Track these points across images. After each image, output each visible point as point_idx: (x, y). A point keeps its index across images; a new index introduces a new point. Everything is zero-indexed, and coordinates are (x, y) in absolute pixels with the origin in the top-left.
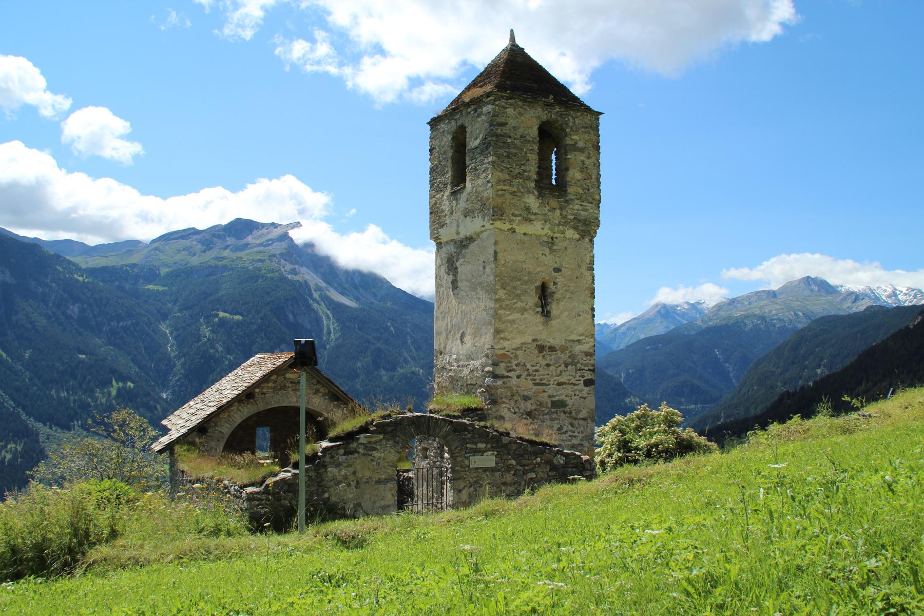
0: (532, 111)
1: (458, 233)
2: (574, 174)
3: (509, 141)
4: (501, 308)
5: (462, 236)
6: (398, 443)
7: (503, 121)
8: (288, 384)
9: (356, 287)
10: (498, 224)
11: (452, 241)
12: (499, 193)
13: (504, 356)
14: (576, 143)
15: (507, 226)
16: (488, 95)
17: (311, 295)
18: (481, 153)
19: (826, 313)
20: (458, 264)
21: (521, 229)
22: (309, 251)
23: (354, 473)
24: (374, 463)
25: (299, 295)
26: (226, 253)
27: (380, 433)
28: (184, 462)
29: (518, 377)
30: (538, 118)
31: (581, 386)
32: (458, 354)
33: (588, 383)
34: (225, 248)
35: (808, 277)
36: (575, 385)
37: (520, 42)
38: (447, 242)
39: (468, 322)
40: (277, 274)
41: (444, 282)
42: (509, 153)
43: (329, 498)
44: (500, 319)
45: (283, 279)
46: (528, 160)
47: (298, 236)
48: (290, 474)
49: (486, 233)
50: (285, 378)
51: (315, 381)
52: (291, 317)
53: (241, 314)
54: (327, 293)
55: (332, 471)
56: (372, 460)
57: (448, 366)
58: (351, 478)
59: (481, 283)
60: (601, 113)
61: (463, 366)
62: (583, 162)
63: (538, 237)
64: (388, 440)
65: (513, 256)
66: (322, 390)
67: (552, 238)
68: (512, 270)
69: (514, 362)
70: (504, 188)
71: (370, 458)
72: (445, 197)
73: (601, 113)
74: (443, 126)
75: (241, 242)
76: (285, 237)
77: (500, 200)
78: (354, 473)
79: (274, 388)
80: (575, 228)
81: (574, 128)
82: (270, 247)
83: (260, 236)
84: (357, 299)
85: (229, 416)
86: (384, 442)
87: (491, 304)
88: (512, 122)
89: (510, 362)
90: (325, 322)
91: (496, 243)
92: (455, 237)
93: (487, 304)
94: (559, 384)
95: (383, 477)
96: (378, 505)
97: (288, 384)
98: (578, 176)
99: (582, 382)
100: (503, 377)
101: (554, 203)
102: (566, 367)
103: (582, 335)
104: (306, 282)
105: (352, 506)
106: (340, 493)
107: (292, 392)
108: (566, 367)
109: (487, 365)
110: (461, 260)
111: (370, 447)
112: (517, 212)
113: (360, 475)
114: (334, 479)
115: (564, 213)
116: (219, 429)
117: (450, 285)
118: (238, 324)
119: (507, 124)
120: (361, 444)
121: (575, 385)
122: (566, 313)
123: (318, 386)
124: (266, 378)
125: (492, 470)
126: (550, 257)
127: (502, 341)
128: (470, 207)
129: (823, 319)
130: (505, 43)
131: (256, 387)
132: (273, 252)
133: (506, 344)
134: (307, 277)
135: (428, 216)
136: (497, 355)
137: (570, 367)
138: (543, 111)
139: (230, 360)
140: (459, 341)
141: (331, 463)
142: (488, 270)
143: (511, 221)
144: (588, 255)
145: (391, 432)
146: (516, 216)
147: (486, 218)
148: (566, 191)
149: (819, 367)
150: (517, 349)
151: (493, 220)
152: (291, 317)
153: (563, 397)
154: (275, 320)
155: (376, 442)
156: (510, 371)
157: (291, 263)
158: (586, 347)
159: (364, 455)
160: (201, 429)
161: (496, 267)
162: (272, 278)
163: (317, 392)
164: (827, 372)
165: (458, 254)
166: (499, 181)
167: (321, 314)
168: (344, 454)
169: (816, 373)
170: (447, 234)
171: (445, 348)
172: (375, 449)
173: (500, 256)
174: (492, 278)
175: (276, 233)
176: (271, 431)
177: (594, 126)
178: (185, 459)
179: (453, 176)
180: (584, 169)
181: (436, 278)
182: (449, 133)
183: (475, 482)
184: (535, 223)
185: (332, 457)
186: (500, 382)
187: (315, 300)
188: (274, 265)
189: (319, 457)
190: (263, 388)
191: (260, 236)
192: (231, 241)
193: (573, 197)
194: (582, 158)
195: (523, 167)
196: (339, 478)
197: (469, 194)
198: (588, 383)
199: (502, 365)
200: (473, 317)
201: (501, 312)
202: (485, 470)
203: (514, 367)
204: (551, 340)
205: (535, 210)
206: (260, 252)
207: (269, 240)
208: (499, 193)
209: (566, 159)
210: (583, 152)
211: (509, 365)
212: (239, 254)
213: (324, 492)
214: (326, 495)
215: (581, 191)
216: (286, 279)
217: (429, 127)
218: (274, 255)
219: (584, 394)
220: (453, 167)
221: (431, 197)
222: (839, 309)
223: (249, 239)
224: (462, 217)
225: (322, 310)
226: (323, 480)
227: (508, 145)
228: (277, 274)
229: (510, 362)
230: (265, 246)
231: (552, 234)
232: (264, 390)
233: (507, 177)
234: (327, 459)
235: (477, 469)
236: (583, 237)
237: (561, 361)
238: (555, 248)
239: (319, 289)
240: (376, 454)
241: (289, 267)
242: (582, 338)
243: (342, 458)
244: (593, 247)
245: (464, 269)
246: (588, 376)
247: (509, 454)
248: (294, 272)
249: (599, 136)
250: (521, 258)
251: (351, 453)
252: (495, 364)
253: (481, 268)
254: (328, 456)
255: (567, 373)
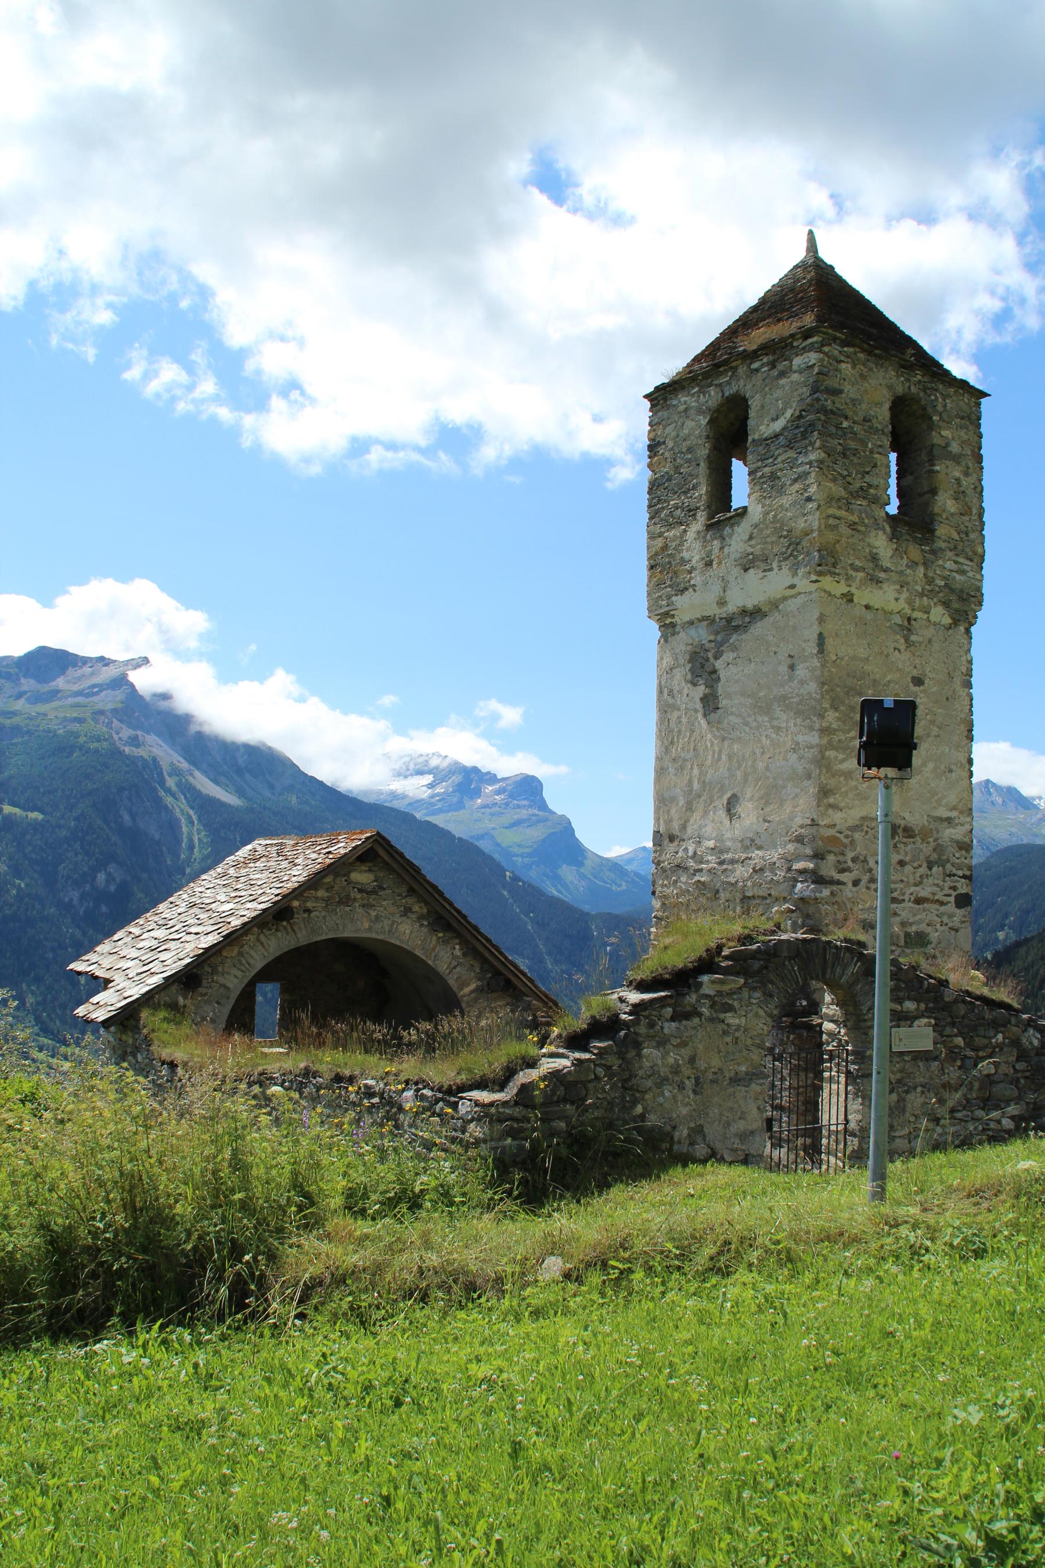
0: (881, 373)
1: (722, 603)
2: (945, 503)
3: (845, 424)
4: (830, 746)
5: (731, 608)
6: (771, 996)
7: (836, 386)
8: (355, 894)
9: (239, 771)
10: (827, 582)
11: (704, 619)
12: (831, 521)
13: (833, 840)
14: (948, 445)
15: (842, 588)
16: (807, 334)
17: (162, 782)
18: (789, 446)
19: (1014, 841)
20: (719, 664)
21: (865, 596)
22: (163, 705)
23: (692, 1060)
24: (728, 1039)
25: (144, 779)
26: (20, 705)
27: (737, 974)
28: (165, 1044)
29: (856, 883)
30: (890, 387)
31: (951, 908)
32: (720, 839)
33: (963, 901)
34: (19, 696)
35: (988, 781)
36: (942, 904)
37: (827, 255)
38: (691, 623)
39: (746, 775)
40: (105, 744)
41: (681, 701)
42: (846, 449)
43: (642, 1117)
44: (828, 768)
45: (116, 753)
46: (875, 466)
47: (142, 680)
48: (566, 1062)
49: (800, 600)
50: (349, 882)
51: (404, 890)
52: (127, 817)
53: (41, 811)
54: (191, 779)
55: (650, 1052)
56: (725, 1033)
57: (691, 863)
58: (687, 1071)
59: (784, 698)
60: (986, 395)
61: (733, 862)
62: (958, 480)
63: (888, 614)
64: (754, 989)
65: (849, 647)
66: (416, 908)
67: (909, 619)
68: (848, 675)
69: (850, 855)
70: (838, 513)
71: (721, 1027)
72: (691, 534)
73: (986, 395)
74: (683, 400)
75: (45, 688)
76: (121, 682)
77: (831, 536)
78: (692, 1060)
79: (327, 901)
80: (946, 604)
81: (945, 416)
82: (95, 699)
83: (79, 679)
84: (240, 793)
85: (241, 954)
86: (745, 993)
87: (814, 738)
88: (850, 391)
89: (843, 854)
90: (185, 829)
91: (821, 619)
92: (713, 610)
93: (800, 738)
94: (919, 901)
95: (743, 1069)
96: (733, 1129)
97: (355, 894)
98: (952, 506)
99: (952, 899)
100: (832, 882)
101: (914, 552)
102: (930, 868)
103: (954, 808)
104: (154, 759)
105: (685, 1132)
106: (669, 1107)
107: (360, 910)
108: (930, 868)
109: (798, 858)
110: (728, 656)
111: (721, 1005)
112: (857, 563)
113: (702, 1064)
114: (653, 1072)
115: (930, 574)
116: (221, 979)
117: (699, 706)
118: (35, 826)
119: (841, 392)
120: (707, 996)
121: (942, 904)
122: (931, 765)
123: (410, 900)
124: (314, 882)
125: (925, 1056)
126: (906, 655)
127: (830, 811)
128: (757, 550)
129: (1010, 849)
130: (799, 254)
131: (296, 898)
132: (100, 706)
133: (837, 817)
134: (156, 751)
135: (644, 573)
136: (822, 838)
137: (935, 869)
138: (898, 376)
139: (19, 888)
140: (722, 814)
141: (651, 1037)
142: (801, 672)
143: (849, 578)
144: (964, 658)
145: (759, 971)
146: (856, 569)
147: (801, 572)
148: (932, 531)
149: (1001, 928)
150: (854, 828)
151: (820, 574)
152: (127, 817)
153: (923, 927)
154: (99, 822)
155: (731, 994)
156: (842, 871)
157: (131, 726)
158: (956, 833)
159: (711, 1020)
160: (189, 978)
161: (823, 666)
162: (97, 751)
163: (407, 911)
164: (1013, 937)
165: (721, 644)
166: (831, 500)
167: (178, 814)
168: (673, 1019)
169: (997, 938)
170: (686, 606)
171: (684, 827)
172: (730, 1008)
173: (829, 643)
174: (813, 687)
175: (107, 674)
176: (284, 991)
177: (974, 417)
178: (166, 1037)
179: (711, 494)
180: (959, 495)
181: (660, 692)
182: (700, 412)
183: (899, 1081)
184: (885, 586)
185: (652, 1025)
186: (826, 892)
187: (169, 791)
188: (101, 729)
189: (626, 1025)
190: (307, 899)
191: (79, 679)
192: (28, 684)
193: (943, 545)
194: (957, 474)
195: (867, 479)
196: (664, 1071)
197: (756, 526)
198: (963, 901)
199: (831, 858)
200: (761, 765)
201: (831, 754)
202: (918, 1056)
203: (850, 863)
204: (907, 815)
205: (886, 563)
206: (78, 705)
207: (94, 686)
208: (831, 521)
209: (932, 471)
210: (958, 463)
211: (841, 858)
212: (41, 708)
213: (634, 1103)
214: (639, 1109)
215: (956, 536)
216: (121, 753)
217: (648, 404)
218: (102, 712)
219: (956, 922)
220: (710, 476)
221: (652, 537)
222: (1036, 836)
223: (60, 683)
224: (736, 571)
225: (180, 808)
226: (633, 1076)
227: (844, 432)
228: (105, 744)
229: (843, 854)
230: (87, 696)
231: (909, 612)
232: (309, 905)
233: (843, 493)
234: (642, 1029)
235: (902, 1053)
236: (956, 623)
237: (922, 857)
238: (913, 638)
239: (176, 772)
240: (731, 1019)
241: (126, 733)
242: (954, 814)
243: (670, 1027)
244: (970, 643)
245: (731, 671)
246: (963, 888)
247: (953, 1024)
248: (135, 742)
249: (980, 436)
250: (862, 652)
251: (687, 1016)
252: (818, 856)
253: (783, 669)
254: (644, 1022)
255: (931, 879)
